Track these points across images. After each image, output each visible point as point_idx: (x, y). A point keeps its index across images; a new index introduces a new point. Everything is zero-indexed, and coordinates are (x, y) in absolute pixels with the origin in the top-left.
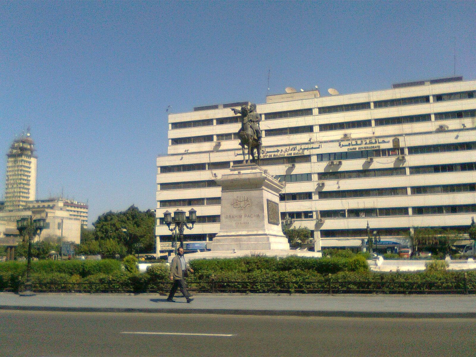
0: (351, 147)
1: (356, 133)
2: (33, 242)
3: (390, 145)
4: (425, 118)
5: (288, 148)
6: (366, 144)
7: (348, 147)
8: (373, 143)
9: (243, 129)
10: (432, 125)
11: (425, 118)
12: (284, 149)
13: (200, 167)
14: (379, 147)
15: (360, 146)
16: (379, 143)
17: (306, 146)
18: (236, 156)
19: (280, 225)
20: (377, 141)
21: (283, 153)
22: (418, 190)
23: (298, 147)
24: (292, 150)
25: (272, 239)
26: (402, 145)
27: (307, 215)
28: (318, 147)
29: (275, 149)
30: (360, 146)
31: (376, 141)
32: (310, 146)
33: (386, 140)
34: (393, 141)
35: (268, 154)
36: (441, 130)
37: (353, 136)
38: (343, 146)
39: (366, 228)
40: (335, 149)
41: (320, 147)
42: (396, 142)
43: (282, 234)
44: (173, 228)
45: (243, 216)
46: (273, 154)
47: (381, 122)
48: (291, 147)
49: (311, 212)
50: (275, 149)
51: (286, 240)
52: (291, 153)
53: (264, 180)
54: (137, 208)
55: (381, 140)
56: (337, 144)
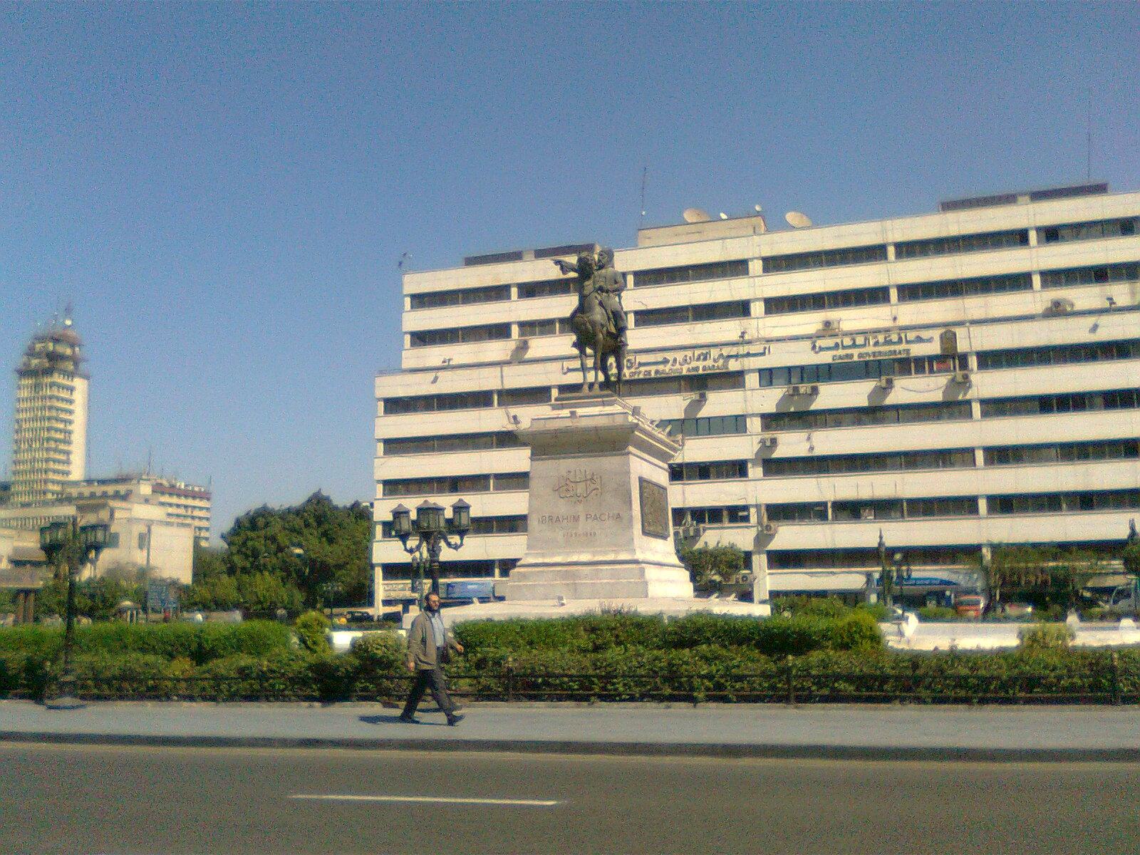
0: (841, 352)
1: (852, 319)
2: (80, 579)
3: (934, 348)
4: (1018, 282)
5: (689, 353)
6: (876, 344)
7: (834, 353)
8: (894, 343)
9: (582, 309)
10: (1035, 299)
11: (1018, 282)
12: (679, 356)
13: (480, 399)
14: (908, 351)
15: (863, 350)
16: (908, 342)
17: (734, 350)
18: (565, 374)
19: (671, 539)
20: (903, 337)
21: (677, 366)
22: (1001, 455)
23: (714, 353)
24: (698, 359)
25: (651, 573)
26: (962, 346)
27: (736, 514)
28: (762, 351)
29: (659, 357)
30: (863, 350)
31: (900, 339)
32: (742, 350)
33: (925, 334)
34: (942, 337)
35: (643, 369)
36: (1057, 311)
37: (846, 326)
38: (821, 349)
39: (876, 545)
40: (803, 356)
41: (767, 351)
42: (949, 339)
43: (675, 560)
44: (414, 547)
45: (582, 518)
46: (653, 369)
47: (912, 292)
48: (697, 352)
49: (745, 508)
50: (659, 357)
51: (686, 575)
52: (698, 367)
53: (633, 432)
54: (327, 499)
55: (911, 335)
56: (808, 344)
